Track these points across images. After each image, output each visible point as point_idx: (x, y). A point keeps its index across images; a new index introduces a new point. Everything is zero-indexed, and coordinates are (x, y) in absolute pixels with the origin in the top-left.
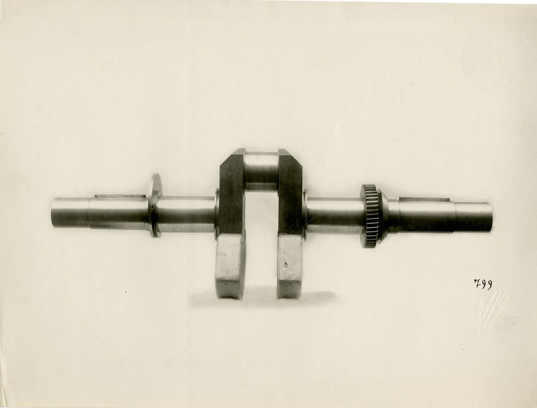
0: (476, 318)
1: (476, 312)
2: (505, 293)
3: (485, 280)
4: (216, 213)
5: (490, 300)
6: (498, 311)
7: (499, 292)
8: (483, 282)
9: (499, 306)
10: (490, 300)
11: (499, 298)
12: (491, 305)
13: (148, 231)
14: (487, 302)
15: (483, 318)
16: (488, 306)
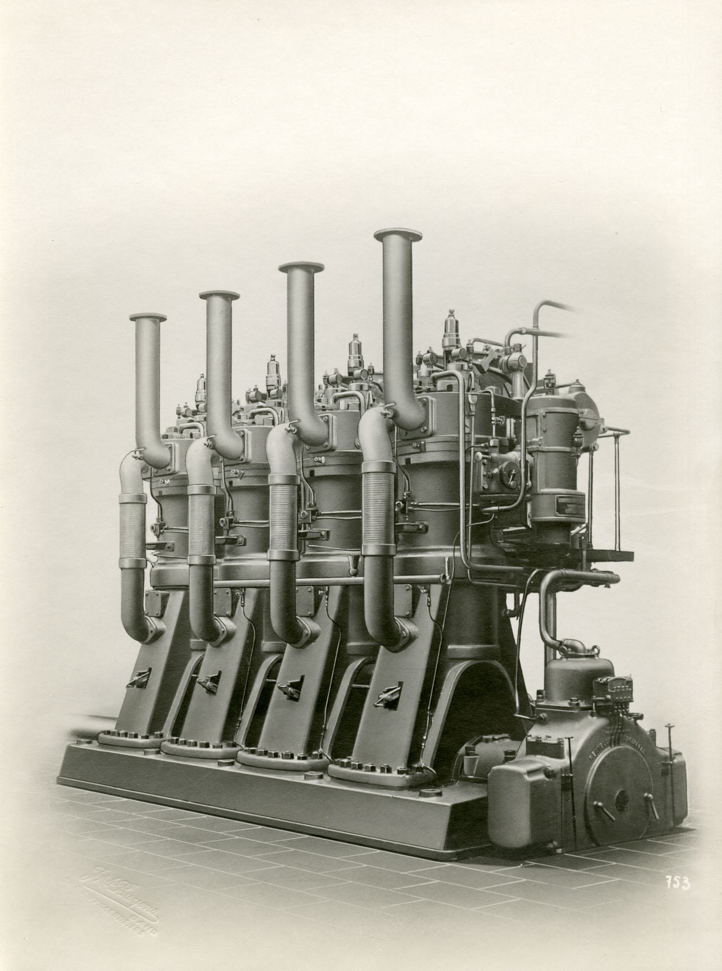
2: (151, 932)
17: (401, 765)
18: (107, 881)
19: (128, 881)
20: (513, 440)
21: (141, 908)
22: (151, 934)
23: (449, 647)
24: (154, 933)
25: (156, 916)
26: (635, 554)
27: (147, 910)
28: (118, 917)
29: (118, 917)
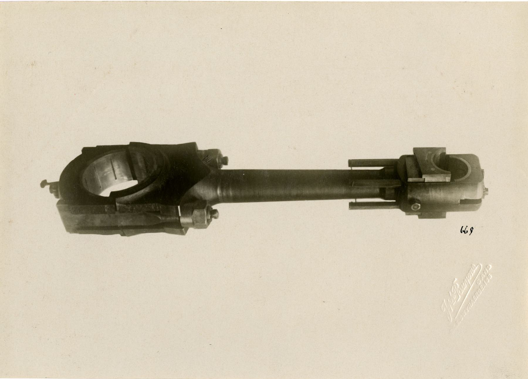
1: (449, 292)
2: (488, 269)
5: (468, 277)
7: (481, 267)
10: (468, 277)
14: (464, 280)
15: (458, 301)
17: (400, 185)
18: (452, 301)
19: (441, 305)
20: (177, 220)
21: (471, 277)
22: (489, 269)
23: (401, 185)
24: (489, 268)
25: (477, 266)
26: (351, 158)
27: (473, 273)
28: (477, 293)
29: (477, 293)
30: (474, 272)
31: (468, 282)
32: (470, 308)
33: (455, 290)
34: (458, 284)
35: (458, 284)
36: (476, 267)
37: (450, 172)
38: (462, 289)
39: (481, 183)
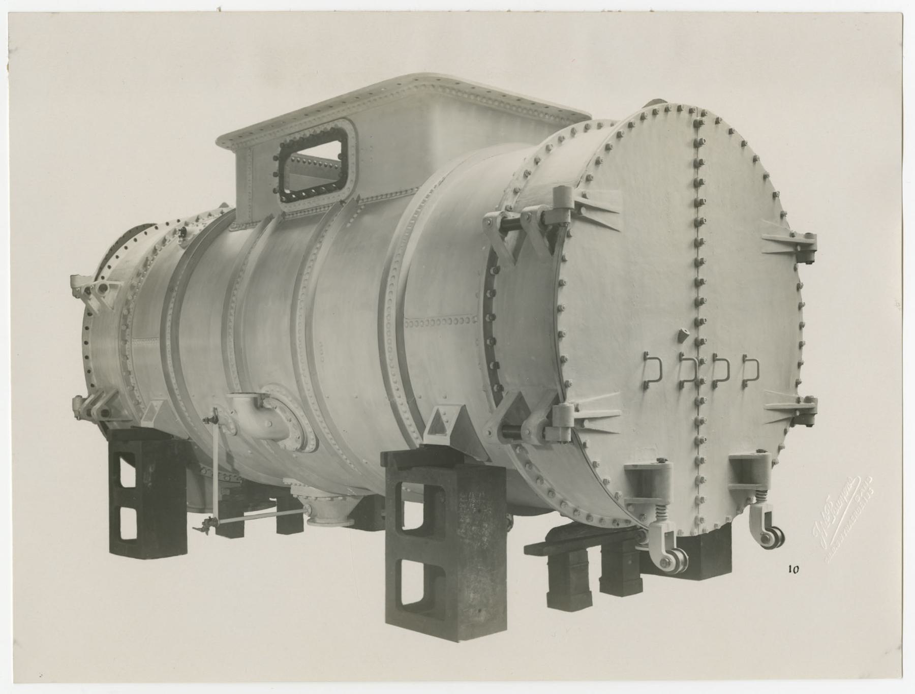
0: (821, 523)
1: (821, 513)
2: (868, 482)
3: (799, 568)
4: (246, 258)
5: (844, 494)
6: (858, 513)
7: (859, 482)
8: (797, 572)
9: (859, 503)
10: (844, 494)
11: (859, 491)
12: (845, 501)
13: (78, 299)
14: (839, 497)
15: (833, 523)
16: (816, 534)
19: (824, 507)
28: (857, 513)
29: (857, 513)
30: (851, 487)
31: (844, 498)
32: (848, 531)
33: (828, 510)
34: (831, 503)
35: (831, 503)
36: (848, 502)
37: (509, 517)
38: (837, 508)
39: (717, 528)
